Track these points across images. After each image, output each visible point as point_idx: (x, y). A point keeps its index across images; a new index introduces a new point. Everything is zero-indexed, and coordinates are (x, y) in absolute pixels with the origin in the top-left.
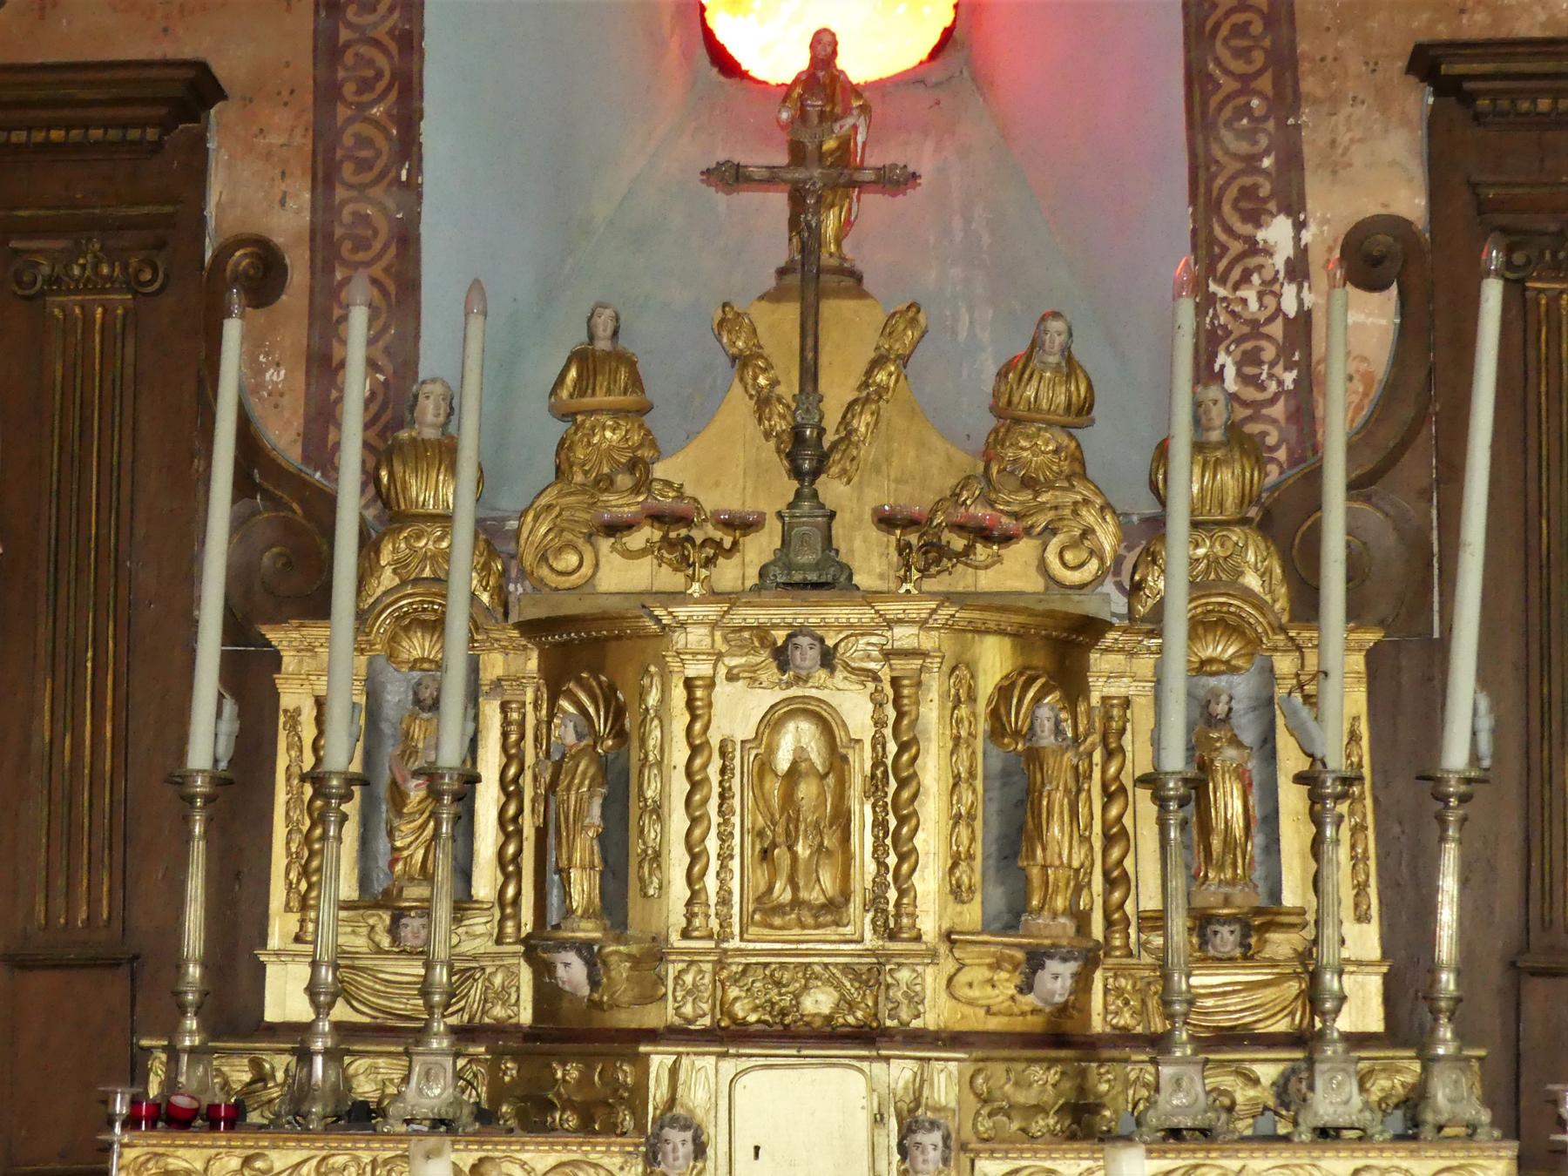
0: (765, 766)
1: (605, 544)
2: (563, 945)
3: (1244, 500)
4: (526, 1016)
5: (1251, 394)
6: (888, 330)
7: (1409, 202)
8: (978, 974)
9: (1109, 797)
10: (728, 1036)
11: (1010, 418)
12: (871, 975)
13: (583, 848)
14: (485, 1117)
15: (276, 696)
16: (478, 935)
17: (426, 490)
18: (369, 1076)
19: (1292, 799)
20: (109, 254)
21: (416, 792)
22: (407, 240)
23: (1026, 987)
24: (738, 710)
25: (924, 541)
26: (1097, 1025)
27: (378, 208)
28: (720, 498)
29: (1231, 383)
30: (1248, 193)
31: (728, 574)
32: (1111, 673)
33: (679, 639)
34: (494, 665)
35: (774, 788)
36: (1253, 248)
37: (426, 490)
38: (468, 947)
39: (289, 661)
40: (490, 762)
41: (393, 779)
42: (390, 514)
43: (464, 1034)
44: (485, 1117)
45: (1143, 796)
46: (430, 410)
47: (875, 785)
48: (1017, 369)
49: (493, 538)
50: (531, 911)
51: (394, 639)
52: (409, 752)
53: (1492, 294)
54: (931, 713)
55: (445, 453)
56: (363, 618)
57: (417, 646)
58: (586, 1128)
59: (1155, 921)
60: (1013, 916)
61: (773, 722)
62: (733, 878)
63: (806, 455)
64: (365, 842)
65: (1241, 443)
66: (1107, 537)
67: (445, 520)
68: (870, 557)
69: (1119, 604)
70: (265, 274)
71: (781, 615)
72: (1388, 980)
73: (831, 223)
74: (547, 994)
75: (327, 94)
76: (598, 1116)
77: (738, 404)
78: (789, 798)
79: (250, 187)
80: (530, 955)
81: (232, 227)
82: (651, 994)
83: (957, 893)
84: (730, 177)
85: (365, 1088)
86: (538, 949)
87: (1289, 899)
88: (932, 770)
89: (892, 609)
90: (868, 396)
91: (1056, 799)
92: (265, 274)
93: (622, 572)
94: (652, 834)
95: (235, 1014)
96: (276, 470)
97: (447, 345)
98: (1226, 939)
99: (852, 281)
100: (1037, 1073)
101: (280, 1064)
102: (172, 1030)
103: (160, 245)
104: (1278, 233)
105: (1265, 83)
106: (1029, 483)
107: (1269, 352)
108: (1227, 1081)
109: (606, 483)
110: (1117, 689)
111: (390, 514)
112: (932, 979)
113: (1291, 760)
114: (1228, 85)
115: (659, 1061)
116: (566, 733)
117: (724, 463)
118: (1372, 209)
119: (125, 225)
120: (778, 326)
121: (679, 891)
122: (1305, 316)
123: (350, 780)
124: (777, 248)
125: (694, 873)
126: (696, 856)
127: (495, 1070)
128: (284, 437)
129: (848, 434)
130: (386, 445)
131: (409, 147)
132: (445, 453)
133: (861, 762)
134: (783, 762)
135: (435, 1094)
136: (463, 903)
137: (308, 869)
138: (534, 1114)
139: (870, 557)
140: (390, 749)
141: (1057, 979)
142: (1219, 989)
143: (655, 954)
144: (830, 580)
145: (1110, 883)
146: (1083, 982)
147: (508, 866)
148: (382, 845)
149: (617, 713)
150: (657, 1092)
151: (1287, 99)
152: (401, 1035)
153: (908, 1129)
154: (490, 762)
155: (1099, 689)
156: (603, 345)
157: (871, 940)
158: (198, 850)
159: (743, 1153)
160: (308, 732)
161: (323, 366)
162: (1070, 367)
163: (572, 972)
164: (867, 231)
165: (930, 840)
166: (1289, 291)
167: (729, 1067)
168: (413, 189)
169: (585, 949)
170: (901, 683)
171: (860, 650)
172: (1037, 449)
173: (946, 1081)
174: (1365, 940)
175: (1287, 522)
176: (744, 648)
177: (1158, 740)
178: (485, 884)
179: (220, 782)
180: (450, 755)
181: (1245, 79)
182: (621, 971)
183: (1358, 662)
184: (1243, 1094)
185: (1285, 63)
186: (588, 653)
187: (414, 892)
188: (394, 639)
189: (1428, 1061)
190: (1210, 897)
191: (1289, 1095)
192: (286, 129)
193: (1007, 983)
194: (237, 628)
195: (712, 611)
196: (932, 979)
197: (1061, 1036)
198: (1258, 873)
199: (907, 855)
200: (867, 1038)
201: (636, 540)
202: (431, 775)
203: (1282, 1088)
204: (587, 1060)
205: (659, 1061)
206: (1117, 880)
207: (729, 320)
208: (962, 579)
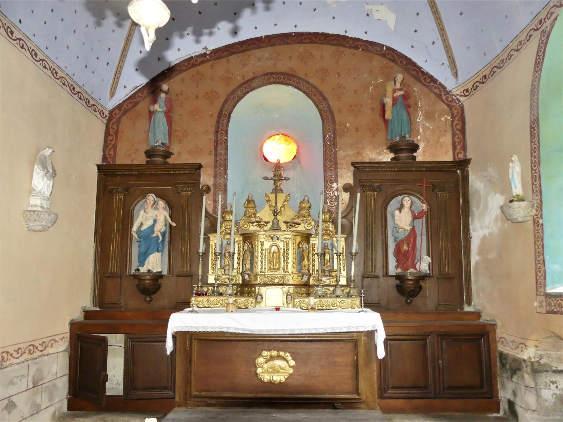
0: (270, 252)
1: (251, 224)
2: (246, 274)
3: (330, 219)
4: (241, 282)
5: (331, 205)
6: (286, 197)
7: (351, 181)
8: (296, 277)
9: (313, 256)
10: (265, 284)
11: (301, 208)
12: (283, 277)
13: (248, 261)
14: (236, 294)
15: (209, 243)
16: (234, 273)
17: (228, 217)
18: (222, 290)
19: (335, 255)
20: (188, 187)
21: (227, 255)
22: (226, 185)
23: (302, 279)
24: (267, 245)
25: (290, 224)
26: (311, 284)
27: (222, 181)
28: (266, 219)
29: (329, 204)
30: (331, 180)
31: (266, 228)
32: (313, 240)
33: (260, 236)
34: (237, 239)
35: (271, 254)
36: (332, 187)
37: (228, 217)
38: (234, 274)
39: (211, 238)
40: (236, 251)
41: (225, 254)
42: (224, 220)
43: (233, 285)
44: (236, 294)
45: (316, 255)
46: (229, 207)
47: (283, 254)
48: (302, 202)
49: (237, 223)
50: (110, 371)
51: (224, 236)
52: (226, 250)
53: (359, 194)
54: (290, 246)
55: (231, 212)
56: (221, 233)
57: (227, 236)
58: (248, 296)
59: (318, 271)
60: (300, 270)
61: (271, 246)
62: (266, 265)
63: (275, 213)
64: (221, 261)
65: (330, 212)
66: (313, 223)
67: (231, 221)
68: (283, 227)
69: (314, 231)
70: (208, 189)
71: (272, 233)
72: (347, 278)
73: (279, 184)
74: (243, 280)
75: (215, 167)
76: (249, 294)
77: (267, 206)
78: (273, 256)
79: (206, 179)
80: (241, 275)
81: (204, 184)
82: (256, 280)
83: (294, 267)
84: (266, 178)
85: (221, 291)
86: (242, 274)
87: (335, 268)
88: (291, 252)
89: (286, 233)
90: (283, 206)
91: (305, 256)
92: (208, 189)
93: (252, 228)
94: (256, 260)
95: (205, 283)
96: (209, 214)
97: (230, 199)
98: (327, 273)
99: (281, 191)
100: (303, 289)
101: (211, 288)
102: (198, 284)
103: (195, 186)
104: (335, 185)
105: (333, 166)
106: (303, 217)
107: (333, 200)
108: (326, 290)
109: (250, 216)
110: (314, 242)
111: (224, 220)
112: (290, 278)
113: (335, 251)
114: (329, 166)
115: (257, 287)
116: (246, 248)
117: (265, 214)
118: (346, 182)
119: (190, 183)
120: (272, 197)
121: (260, 267)
122: (338, 196)
123: (219, 253)
124: (272, 187)
126: (262, 263)
127: (237, 288)
128: (210, 211)
129: (281, 211)
130: (223, 212)
131: (226, 173)
132: (231, 212)
133: (282, 251)
134: (272, 251)
135: (230, 292)
136: (233, 269)
137: (214, 264)
138: (242, 294)
139: (283, 227)
140: (224, 249)
141: (305, 278)
142: (326, 279)
143: (256, 275)
144: (278, 229)
145: (313, 266)
146: (309, 279)
147: (239, 264)
148: (223, 261)
149: (252, 245)
150: (257, 291)
151: (336, 168)
152: (226, 285)
153: (287, 296)
154: (236, 251)
155: (311, 242)
156: (250, 199)
157: (283, 273)
158: (201, 262)
159: (267, 298)
160: (214, 247)
161: (215, 201)
162: (308, 202)
163: (247, 277)
164: (283, 185)
165: (291, 261)
166: (336, 192)
167: (266, 288)
168: (226, 179)
169: (248, 274)
170: (286, 241)
171: (281, 238)
172: (305, 212)
173: (292, 289)
174: (344, 273)
175: (334, 222)
176: (268, 237)
177: (318, 249)
178: (236, 266)
179: (203, 253)
180: (232, 251)
181: (331, 166)
182: (253, 277)
183: (344, 239)
184: (329, 292)
185: (336, 164)
186: (248, 238)
187: (227, 267)
188: (224, 236)
189: (350, 288)
190: (325, 268)
191: (334, 292)
192: (210, 171)
193: (300, 278)
194: (205, 235)
195: (264, 233)
196: (290, 278)
197: (306, 285)
198: (331, 265)
199: (287, 263)
200: (282, 285)
201: (254, 224)
202: (229, 252)
203: (333, 291)
204: (248, 287)
205: (257, 287)
206: (314, 266)
207: (266, 196)
208: (294, 229)
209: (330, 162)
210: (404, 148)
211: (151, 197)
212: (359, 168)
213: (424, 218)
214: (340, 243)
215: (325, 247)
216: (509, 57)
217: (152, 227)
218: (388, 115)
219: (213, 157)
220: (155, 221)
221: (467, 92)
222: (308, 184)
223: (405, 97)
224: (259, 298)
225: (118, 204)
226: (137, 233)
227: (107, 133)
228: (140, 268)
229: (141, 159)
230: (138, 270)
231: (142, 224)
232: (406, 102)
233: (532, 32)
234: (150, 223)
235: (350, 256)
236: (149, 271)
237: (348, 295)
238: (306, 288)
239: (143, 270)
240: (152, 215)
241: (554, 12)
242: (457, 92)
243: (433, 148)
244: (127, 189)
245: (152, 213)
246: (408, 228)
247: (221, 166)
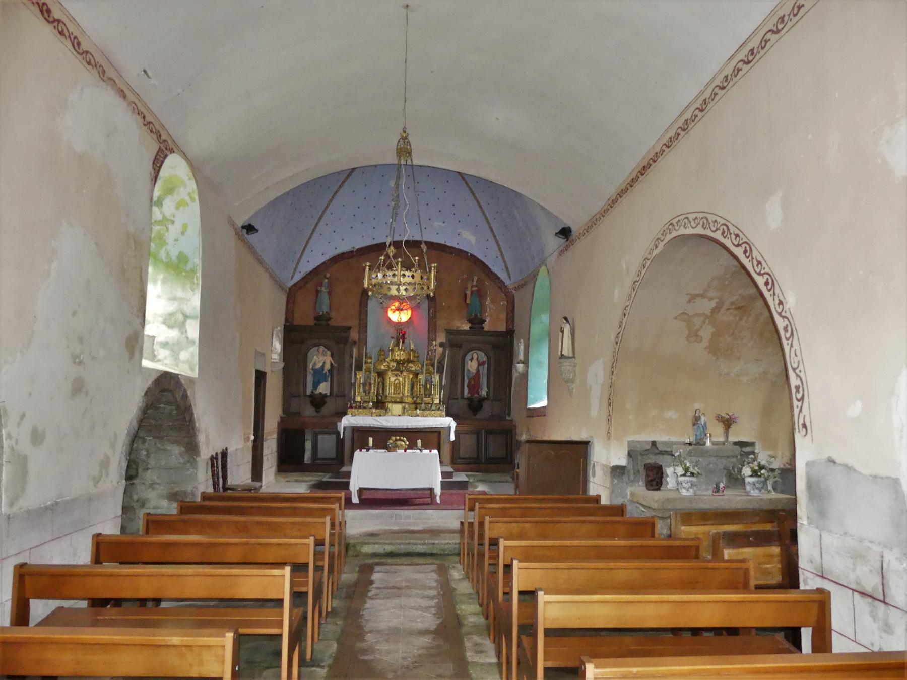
10: (391, 402)
12: (402, 398)
18: (365, 405)
32: (420, 377)
60: (412, 394)
62: (392, 391)
65: (431, 359)
70: (355, 342)
76: (382, 408)
79: (354, 335)
125: (390, 390)
170: (405, 379)
175: (433, 365)
177: (423, 382)
185: (436, 329)
200: (401, 403)
209: (432, 329)
210: (477, 322)
212: (449, 332)
213: (486, 366)
214: (436, 378)
215: (426, 381)
216: (763, 44)
217: (323, 366)
218: (468, 301)
219: (357, 321)
221: (516, 289)
222: (417, 340)
223: (478, 291)
224: (387, 410)
227: (288, 303)
229: (311, 322)
231: (315, 364)
232: (480, 294)
233: (769, 36)
234: (321, 364)
235: (441, 387)
237: (439, 409)
238: (416, 405)
239: (317, 392)
240: (320, 359)
241: (803, 5)
242: (510, 287)
243: (493, 322)
245: (322, 358)
246: (474, 371)
247: (363, 327)
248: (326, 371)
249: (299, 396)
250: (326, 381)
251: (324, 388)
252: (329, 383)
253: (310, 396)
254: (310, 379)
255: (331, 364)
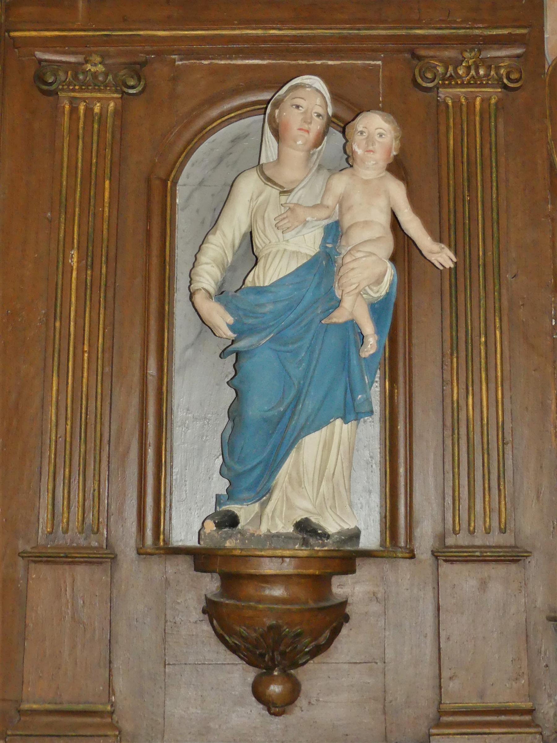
211: (309, 97)
217: (325, 266)
220: (335, 232)
225: (87, 150)
226: (221, 295)
228: (245, 512)
230: (229, 521)
231: (249, 250)
234: (307, 242)
236: (306, 528)
239: (272, 518)
244: (137, 69)
248: (354, 307)
249: (104, 557)
250: (352, 412)
251: (331, 480)
252: (371, 430)
253: (202, 558)
254: (198, 401)
255: (404, 251)
